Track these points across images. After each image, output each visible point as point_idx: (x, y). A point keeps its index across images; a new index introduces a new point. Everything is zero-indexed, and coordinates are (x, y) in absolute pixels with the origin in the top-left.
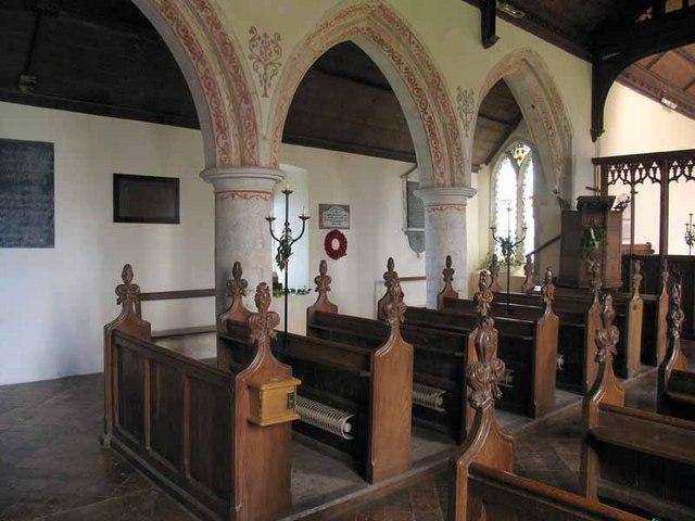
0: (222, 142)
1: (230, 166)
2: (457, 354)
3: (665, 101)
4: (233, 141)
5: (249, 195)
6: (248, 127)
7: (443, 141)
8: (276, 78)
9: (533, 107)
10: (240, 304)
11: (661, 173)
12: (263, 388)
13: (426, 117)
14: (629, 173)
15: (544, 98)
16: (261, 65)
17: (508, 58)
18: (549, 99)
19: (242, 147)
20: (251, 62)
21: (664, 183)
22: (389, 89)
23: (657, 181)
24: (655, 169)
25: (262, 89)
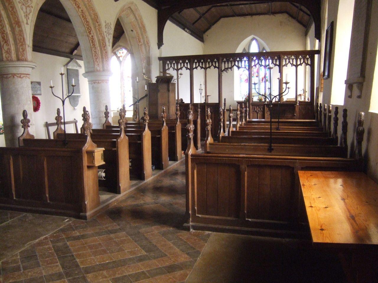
0: (6, 48)
1: (11, 61)
2: (157, 136)
3: (186, 29)
4: (13, 48)
5: (22, 76)
6: (19, 41)
7: (99, 48)
8: (31, 14)
9: (132, 31)
10: (28, 131)
11: (190, 65)
12: (96, 151)
13: (90, 36)
14: (176, 65)
15: (138, 26)
16: (24, 7)
17: (124, 6)
18: (140, 28)
19: (17, 51)
20: (19, 5)
21: (191, 69)
22: (69, 20)
23: (188, 69)
24: (187, 63)
25: (26, 19)
